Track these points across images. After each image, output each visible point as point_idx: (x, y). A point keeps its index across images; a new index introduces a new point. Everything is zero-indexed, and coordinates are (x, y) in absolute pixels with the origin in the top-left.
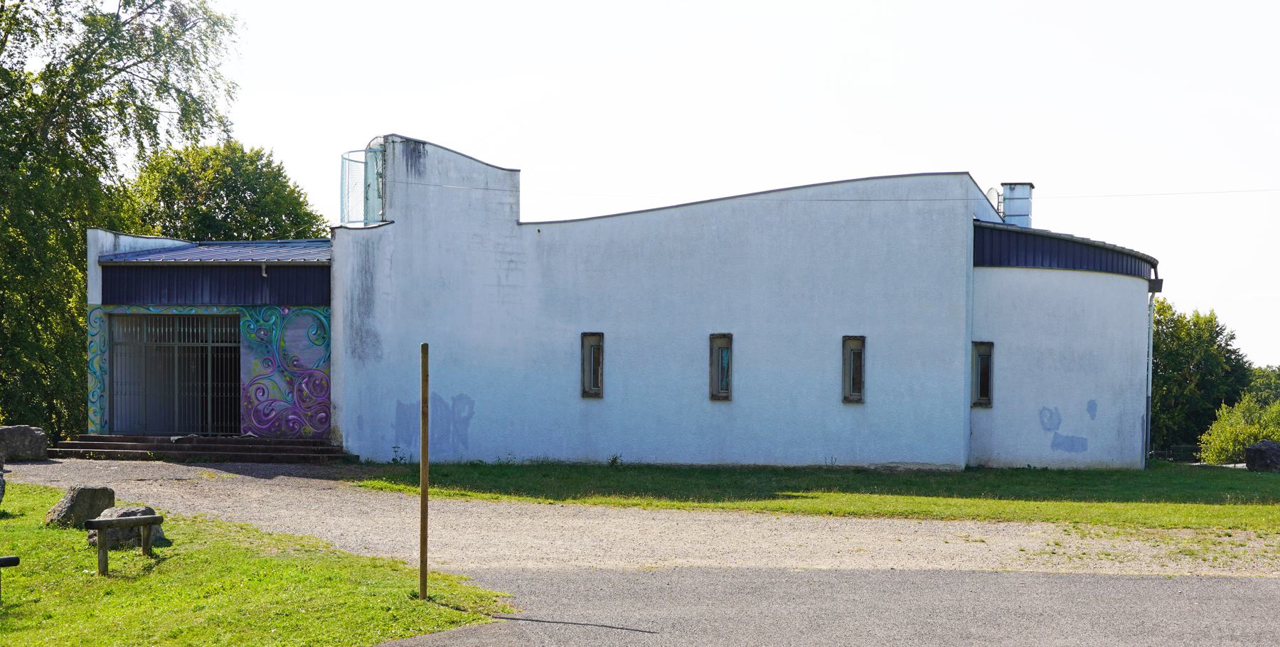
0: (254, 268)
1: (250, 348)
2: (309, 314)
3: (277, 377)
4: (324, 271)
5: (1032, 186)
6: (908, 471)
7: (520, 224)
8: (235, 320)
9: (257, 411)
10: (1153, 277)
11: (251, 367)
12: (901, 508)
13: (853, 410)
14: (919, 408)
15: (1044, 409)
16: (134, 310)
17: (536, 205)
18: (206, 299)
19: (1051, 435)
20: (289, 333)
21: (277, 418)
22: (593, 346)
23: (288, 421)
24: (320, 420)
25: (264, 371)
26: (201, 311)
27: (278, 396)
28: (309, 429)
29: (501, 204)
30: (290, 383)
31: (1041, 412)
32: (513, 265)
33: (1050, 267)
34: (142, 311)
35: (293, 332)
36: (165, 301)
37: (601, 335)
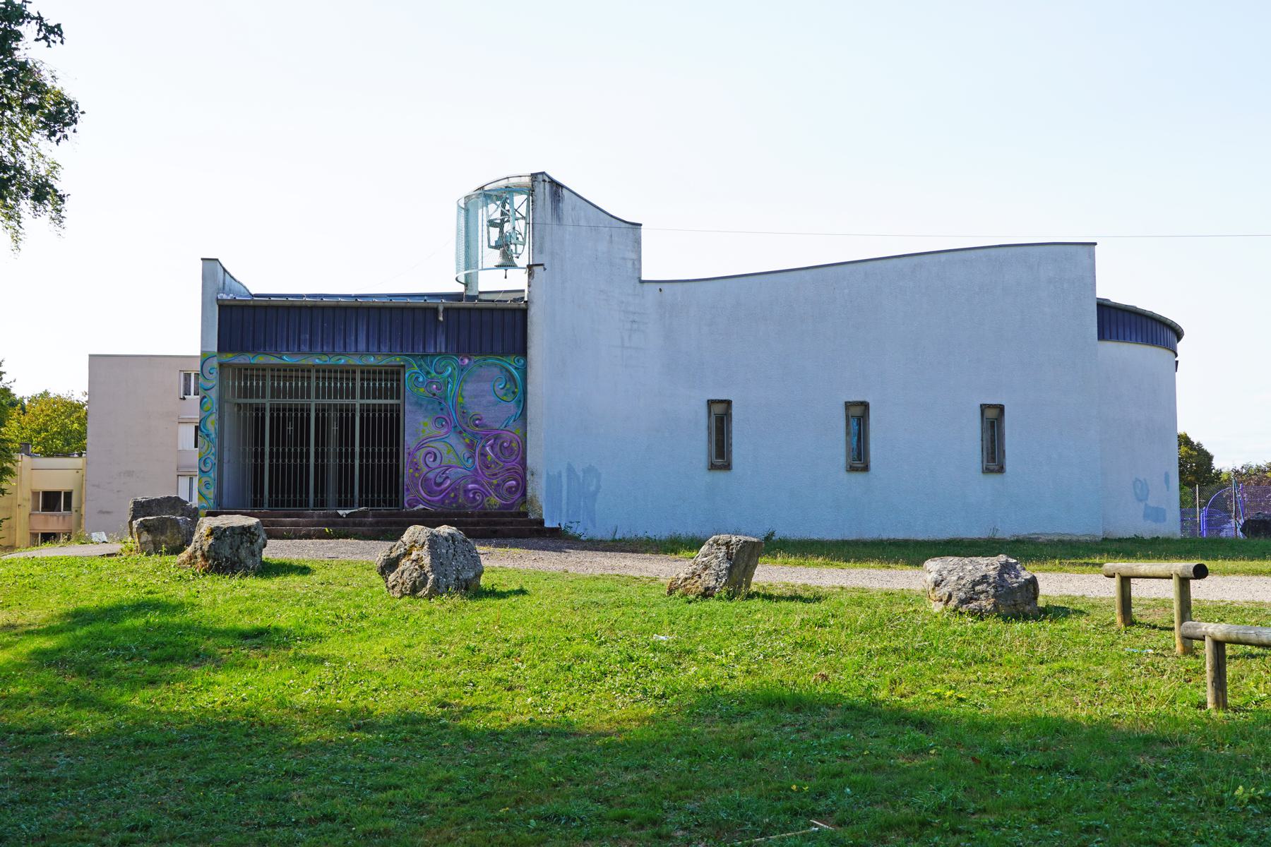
1: (418, 404)
2: (495, 365)
3: (453, 439)
7: (642, 282)
8: (395, 374)
9: (426, 480)
11: (419, 429)
13: (994, 479)
15: (1137, 480)
16: (260, 359)
18: (362, 346)
19: (1142, 505)
20: (470, 387)
21: (453, 488)
22: (721, 417)
23: (466, 491)
24: (509, 490)
25: (436, 432)
26: (353, 361)
27: (454, 462)
28: (494, 501)
29: (624, 259)
30: (471, 446)
31: (1134, 483)
32: (635, 326)
33: (1136, 342)
34: (273, 360)
35: (476, 385)
36: (305, 348)
37: (729, 403)
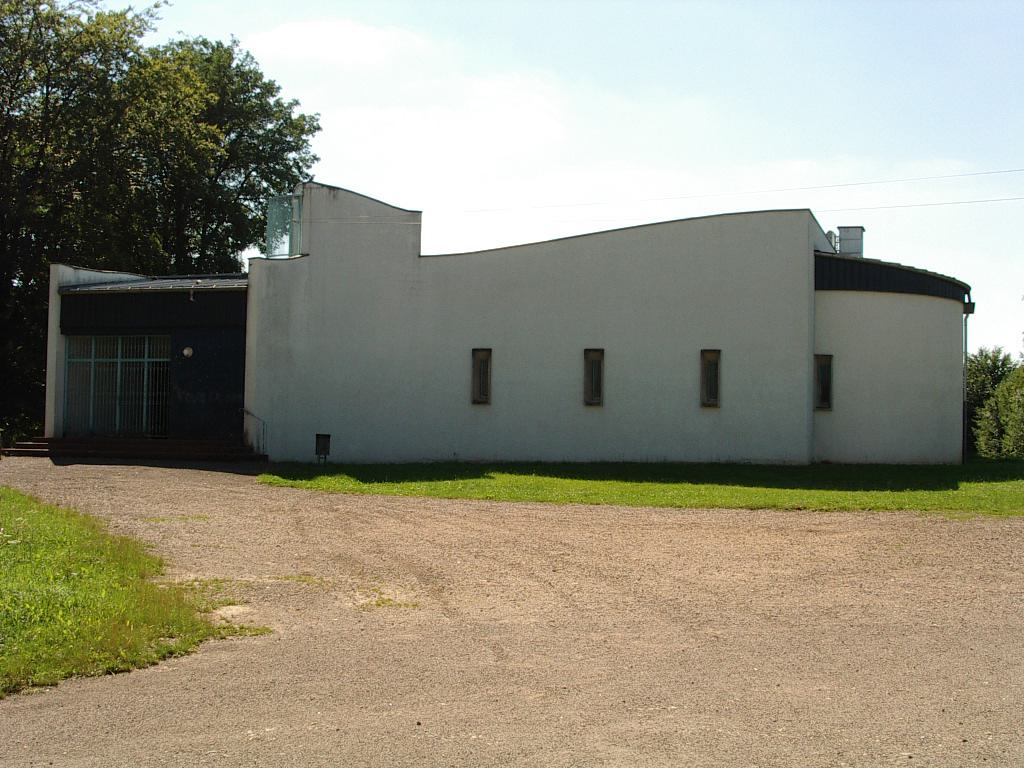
0: (185, 293)
4: (242, 295)
5: (862, 229)
6: (839, 465)
7: (420, 256)
10: (967, 301)
12: (755, 501)
14: (767, 404)
17: (433, 243)
37: (490, 350)
